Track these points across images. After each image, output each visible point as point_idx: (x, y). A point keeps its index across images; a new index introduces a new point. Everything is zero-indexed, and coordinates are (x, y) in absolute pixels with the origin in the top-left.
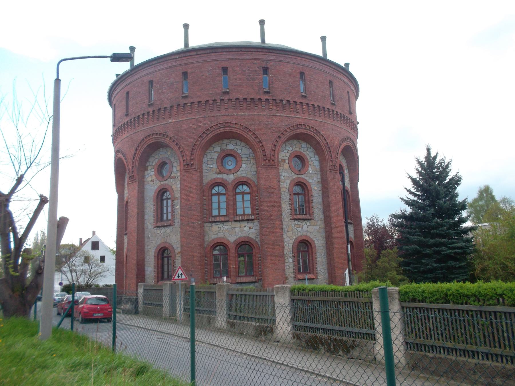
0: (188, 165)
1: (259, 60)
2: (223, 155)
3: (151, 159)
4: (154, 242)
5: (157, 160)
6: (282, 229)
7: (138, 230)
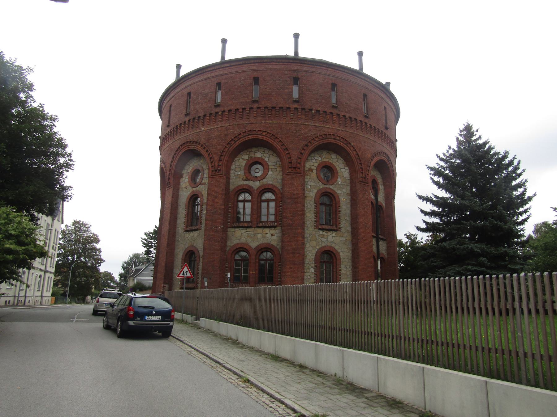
0: (216, 171)
1: (290, 70)
2: (250, 163)
3: (187, 167)
4: (183, 245)
5: (191, 168)
6: (304, 238)
7: (169, 234)
